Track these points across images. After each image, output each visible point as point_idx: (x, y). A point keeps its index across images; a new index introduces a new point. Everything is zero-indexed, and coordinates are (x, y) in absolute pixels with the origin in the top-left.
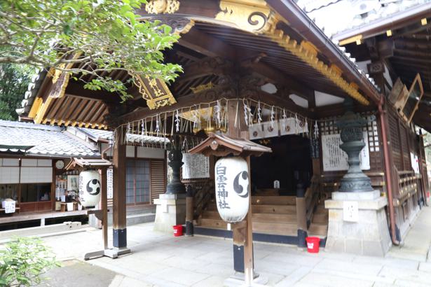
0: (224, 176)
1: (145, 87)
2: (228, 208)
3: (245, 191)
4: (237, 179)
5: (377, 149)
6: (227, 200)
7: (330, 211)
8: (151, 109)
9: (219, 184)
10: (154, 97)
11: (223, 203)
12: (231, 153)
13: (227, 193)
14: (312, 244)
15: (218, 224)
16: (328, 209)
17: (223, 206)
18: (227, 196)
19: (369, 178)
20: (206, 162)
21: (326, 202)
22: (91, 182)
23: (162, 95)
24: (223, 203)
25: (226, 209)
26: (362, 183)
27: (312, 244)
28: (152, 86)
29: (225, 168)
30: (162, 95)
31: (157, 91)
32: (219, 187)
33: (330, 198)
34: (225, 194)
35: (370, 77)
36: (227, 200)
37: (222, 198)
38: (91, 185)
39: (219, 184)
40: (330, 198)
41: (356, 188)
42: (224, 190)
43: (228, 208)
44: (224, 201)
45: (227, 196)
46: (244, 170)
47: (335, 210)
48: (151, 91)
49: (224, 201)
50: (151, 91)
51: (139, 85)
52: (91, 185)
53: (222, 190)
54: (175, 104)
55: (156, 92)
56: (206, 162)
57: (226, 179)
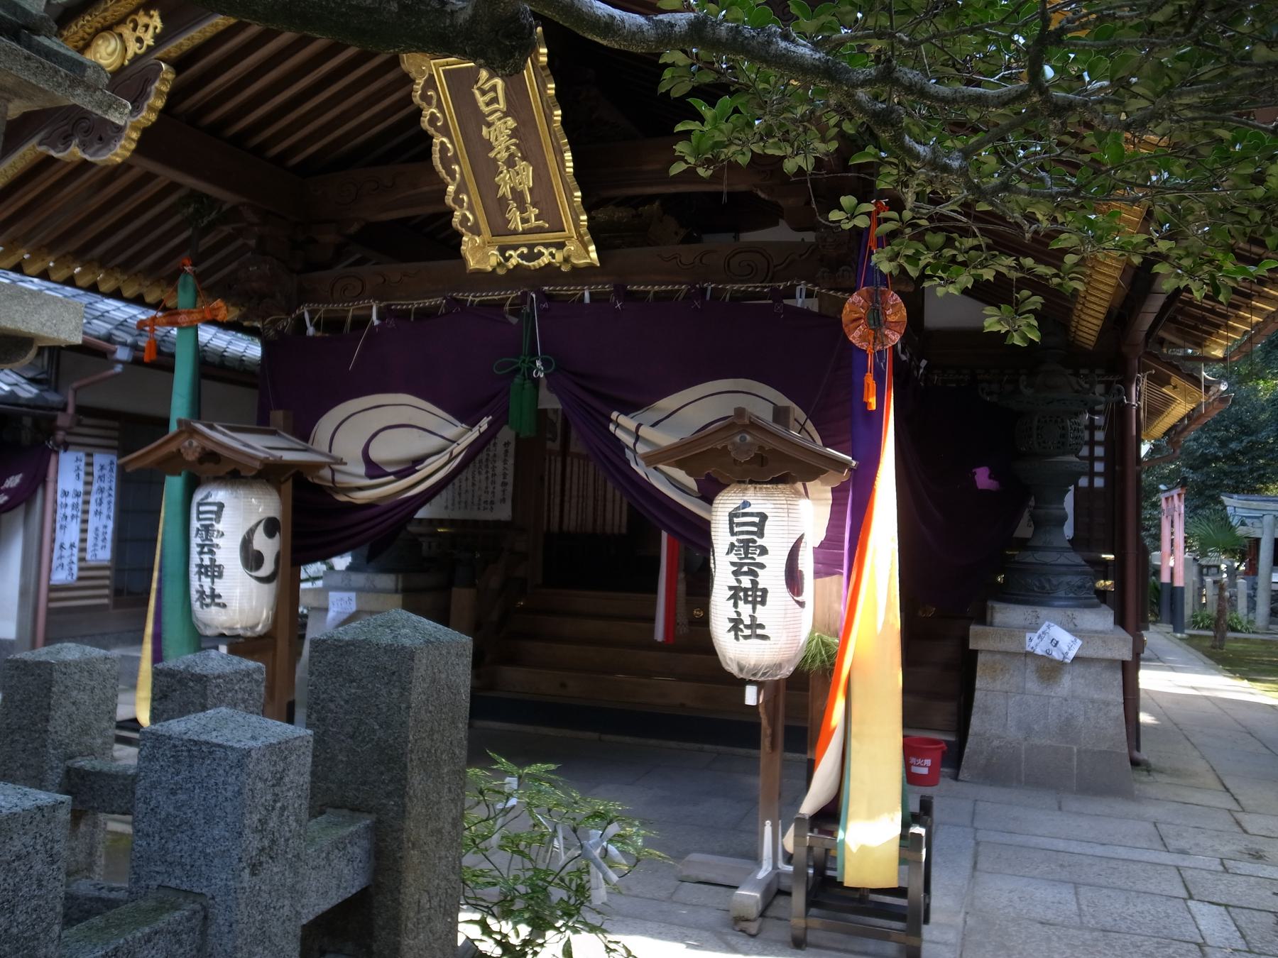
0: (760, 542)
1: (472, 186)
2: (764, 637)
3: (267, 569)
4: (246, 543)
5: (1099, 482)
6: (220, 586)
7: (981, 658)
8: (472, 264)
9: (202, 546)
10: (500, 229)
11: (208, 591)
12: (236, 474)
13: (765, 591)
14: (928, 762)
15: (563, 685)
16: (975, 652)
17: (747, 632)
18: (763, 603)
19: (1088, 569)
20: (499, 465)
21: (974, 629)
22: (260, 529)
23: (539, 230)
24: (747, 621)
25: (214, 609)
26: (1076, 580)
27: (928, 762)
28: (505, 190)
29: (763, 517)
30: (539, 230)
31: (522, 209)
32: (201, 553)
33: (983, 619)
34: (214, 571)
35: (999, 275)
36: (762, 614)
37: (206, 582)
38: (262, 543)
39: (202, 546)
40: (983, 619)
41: (1062, 594)
42: (754, 583)
43: (764, 637)
44: (753, 618)
45: (763, 603)
46: (272, 514)
47: (998, 657)
48: (496, 208)
49: (753, 618)
50: (496, 208)
51: (451, 174)
52: (262, 543)
53: (206, 562)
54: (591, 267)
55: (515, 219)
56: (499, 465)
57: (764, 551)
